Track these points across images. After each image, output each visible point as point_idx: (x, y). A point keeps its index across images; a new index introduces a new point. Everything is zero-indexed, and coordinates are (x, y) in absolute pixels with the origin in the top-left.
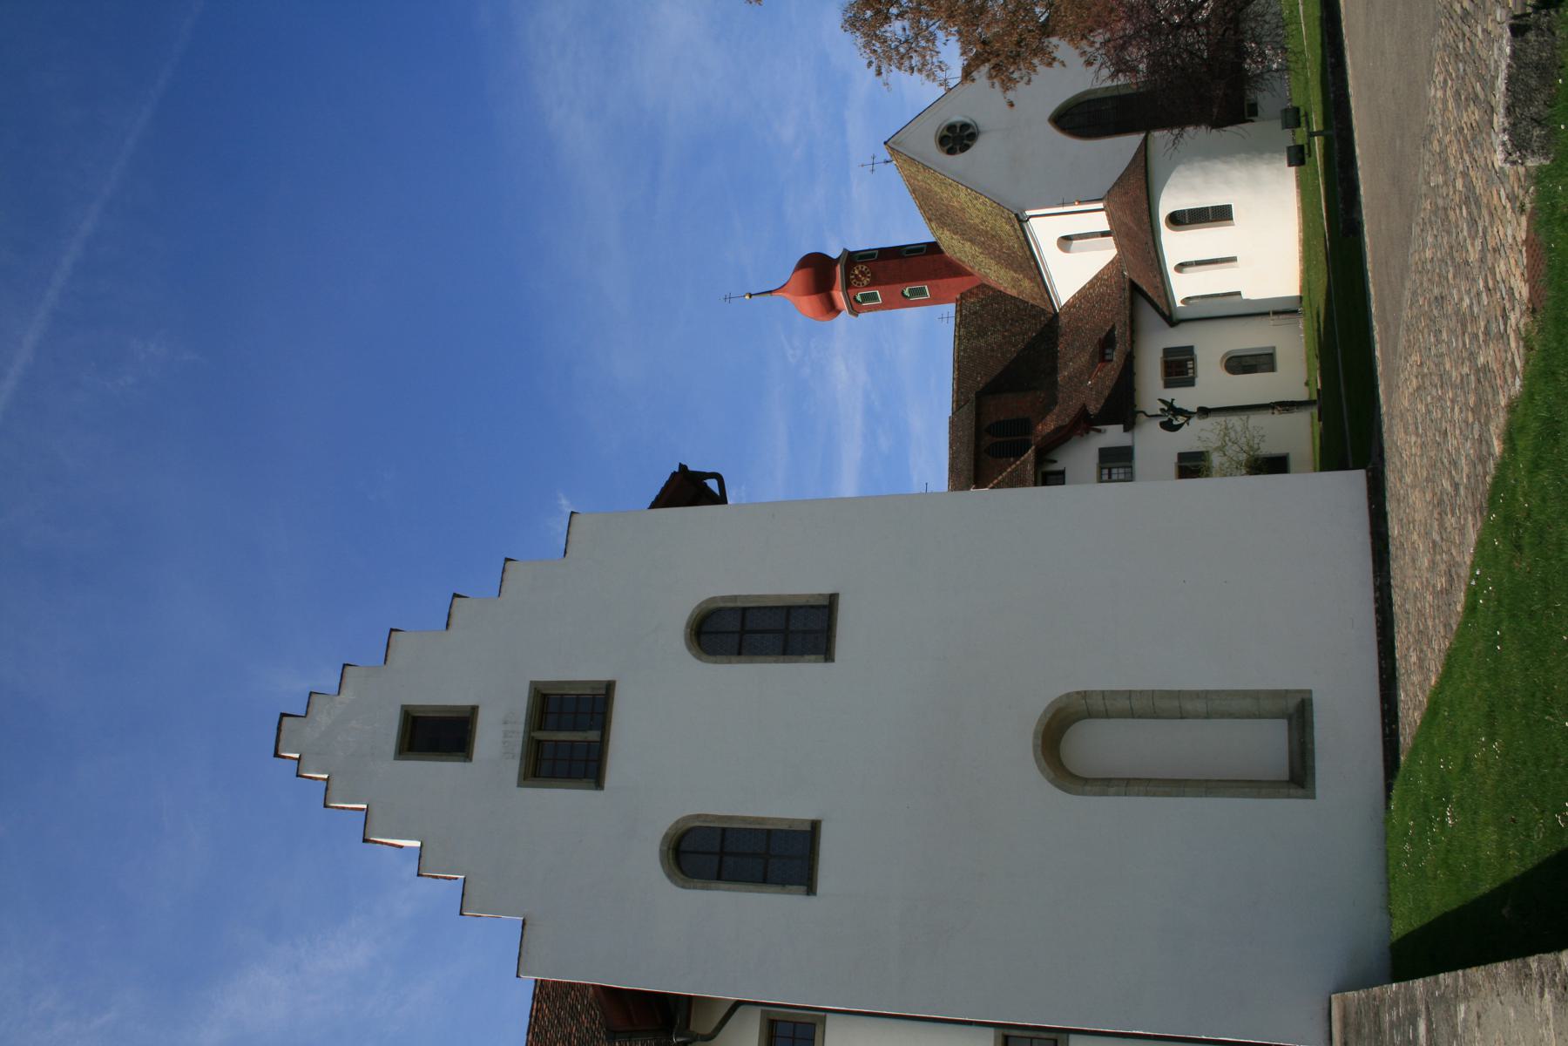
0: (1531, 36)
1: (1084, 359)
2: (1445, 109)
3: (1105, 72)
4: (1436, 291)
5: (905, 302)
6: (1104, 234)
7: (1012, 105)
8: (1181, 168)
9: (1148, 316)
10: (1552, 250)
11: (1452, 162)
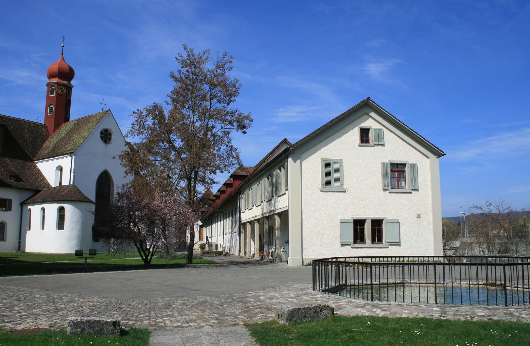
0: (112, 327)
1: (13, 169)
2: (90, 302)
3: (120, 191)
4: (23, 298)
5: (48, 105)
6: (61, 183)
7: (114, 158)
8: (80, 213)
9: (25, 195)
10: (35, 336)
11: (71, 304)
